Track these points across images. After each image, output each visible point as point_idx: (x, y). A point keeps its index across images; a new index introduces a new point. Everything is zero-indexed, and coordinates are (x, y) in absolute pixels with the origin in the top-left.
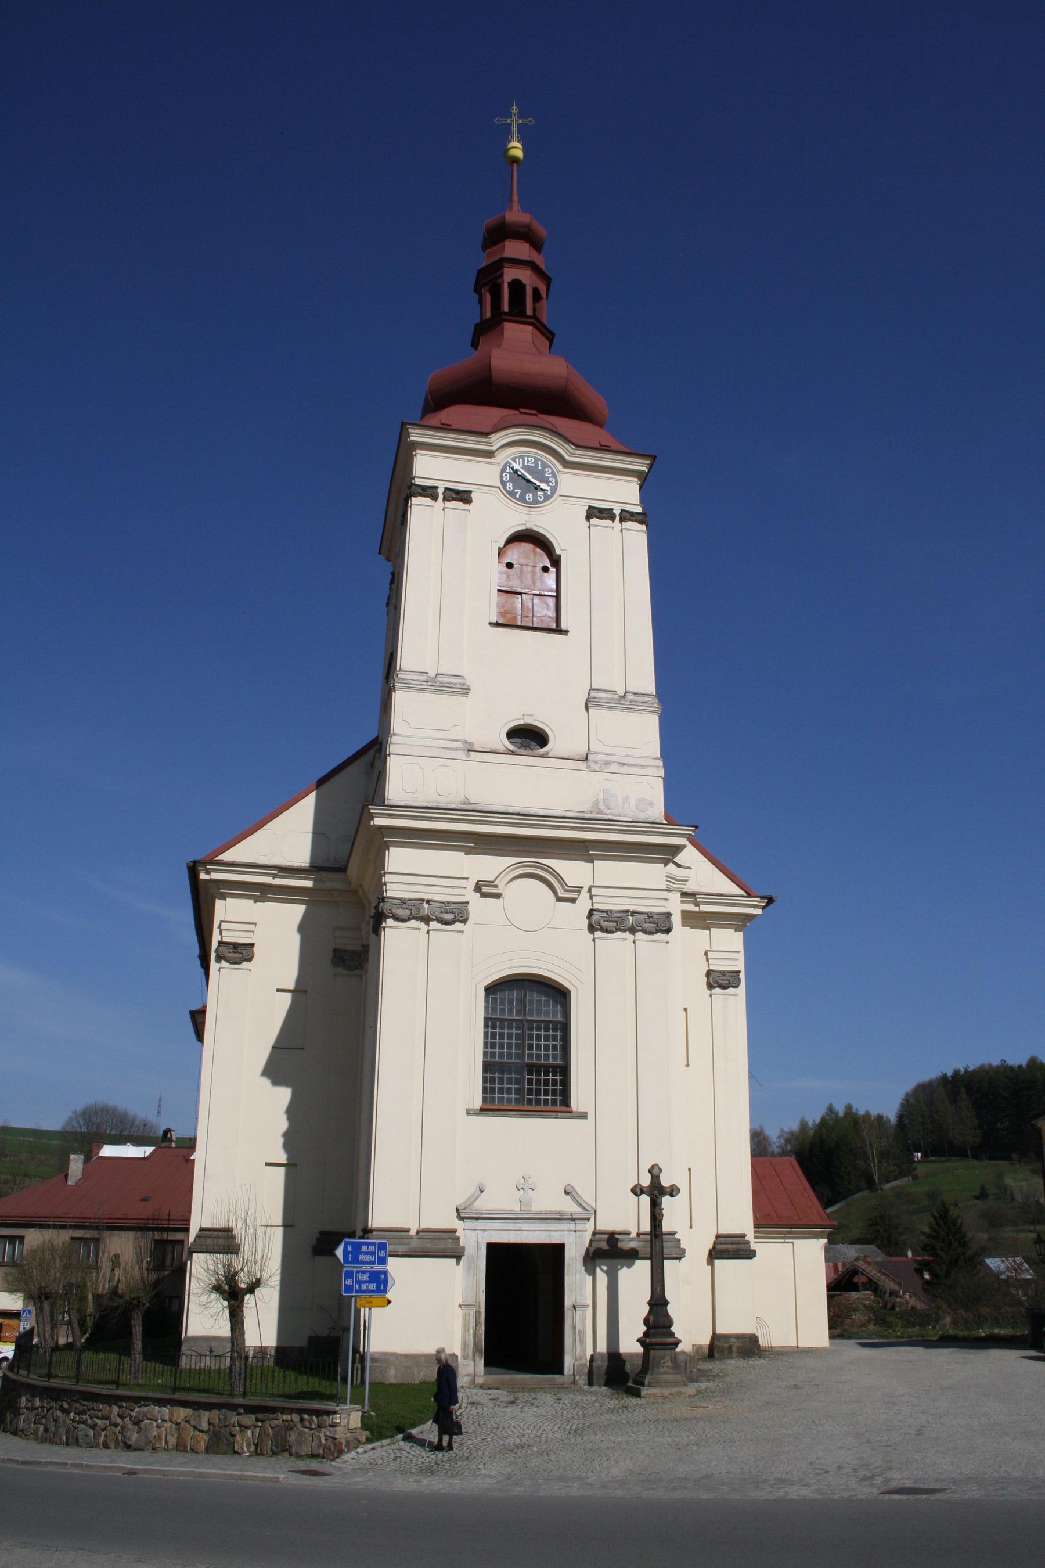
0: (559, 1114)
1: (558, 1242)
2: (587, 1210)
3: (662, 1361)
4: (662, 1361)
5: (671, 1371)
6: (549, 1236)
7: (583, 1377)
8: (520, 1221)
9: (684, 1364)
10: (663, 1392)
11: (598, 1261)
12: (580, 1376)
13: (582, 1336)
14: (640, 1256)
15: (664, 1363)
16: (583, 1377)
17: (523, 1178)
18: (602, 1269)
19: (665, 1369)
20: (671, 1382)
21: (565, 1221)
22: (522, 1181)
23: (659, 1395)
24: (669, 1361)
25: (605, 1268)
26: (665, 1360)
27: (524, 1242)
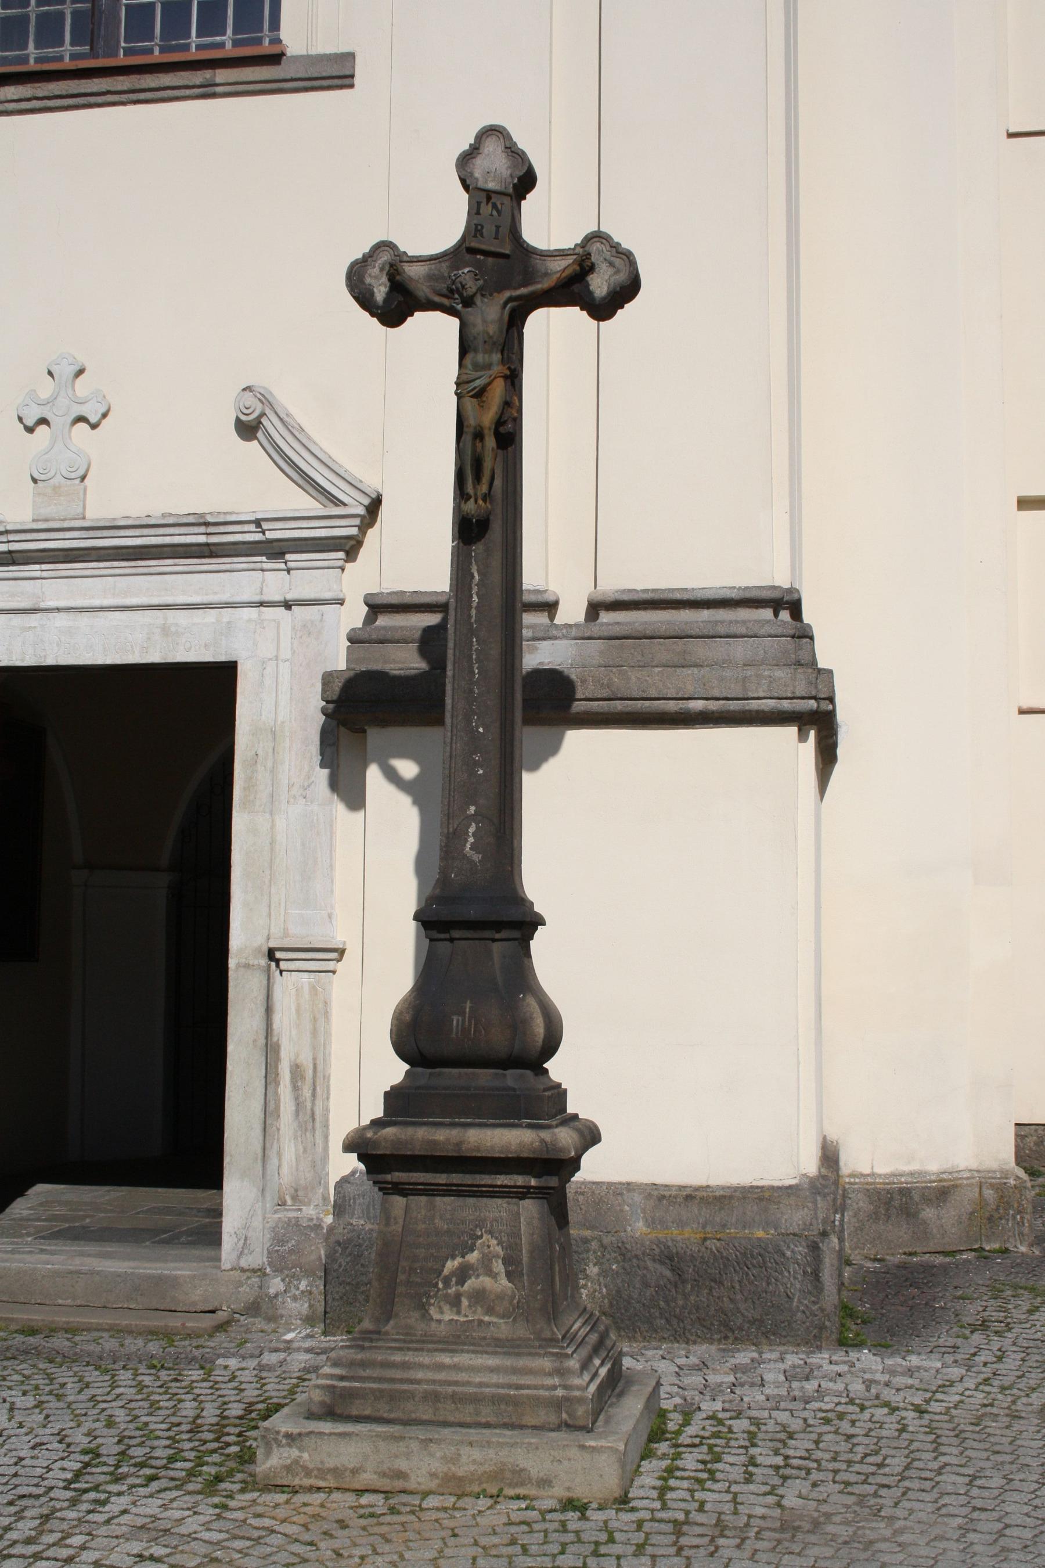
0: (222, 75)
1: (222, 658)
2: (337, 502)
3: (451, 1265)
4: (451, 1265)
5: (502, 1328)
6: (165, 630)
7: (303, 1285)
8: (34, 570)
9: (801, 1249)
10: (402, 1465)
11: (375, 736)
12: (290, 1280)
13: (307, 1093)
14: (578, 707)
15: (463, 1274)
16: (303, 1285)
17: (50, 373)
18: (392, 776)
19: (468, 1314)
20: (476, 1400)
21: (240, 562)
22: (46, 388)
23: (367, 1478)
24: (499, 1267)
25: (408, 769)
26: (473, 1257)
27: (50, 661)
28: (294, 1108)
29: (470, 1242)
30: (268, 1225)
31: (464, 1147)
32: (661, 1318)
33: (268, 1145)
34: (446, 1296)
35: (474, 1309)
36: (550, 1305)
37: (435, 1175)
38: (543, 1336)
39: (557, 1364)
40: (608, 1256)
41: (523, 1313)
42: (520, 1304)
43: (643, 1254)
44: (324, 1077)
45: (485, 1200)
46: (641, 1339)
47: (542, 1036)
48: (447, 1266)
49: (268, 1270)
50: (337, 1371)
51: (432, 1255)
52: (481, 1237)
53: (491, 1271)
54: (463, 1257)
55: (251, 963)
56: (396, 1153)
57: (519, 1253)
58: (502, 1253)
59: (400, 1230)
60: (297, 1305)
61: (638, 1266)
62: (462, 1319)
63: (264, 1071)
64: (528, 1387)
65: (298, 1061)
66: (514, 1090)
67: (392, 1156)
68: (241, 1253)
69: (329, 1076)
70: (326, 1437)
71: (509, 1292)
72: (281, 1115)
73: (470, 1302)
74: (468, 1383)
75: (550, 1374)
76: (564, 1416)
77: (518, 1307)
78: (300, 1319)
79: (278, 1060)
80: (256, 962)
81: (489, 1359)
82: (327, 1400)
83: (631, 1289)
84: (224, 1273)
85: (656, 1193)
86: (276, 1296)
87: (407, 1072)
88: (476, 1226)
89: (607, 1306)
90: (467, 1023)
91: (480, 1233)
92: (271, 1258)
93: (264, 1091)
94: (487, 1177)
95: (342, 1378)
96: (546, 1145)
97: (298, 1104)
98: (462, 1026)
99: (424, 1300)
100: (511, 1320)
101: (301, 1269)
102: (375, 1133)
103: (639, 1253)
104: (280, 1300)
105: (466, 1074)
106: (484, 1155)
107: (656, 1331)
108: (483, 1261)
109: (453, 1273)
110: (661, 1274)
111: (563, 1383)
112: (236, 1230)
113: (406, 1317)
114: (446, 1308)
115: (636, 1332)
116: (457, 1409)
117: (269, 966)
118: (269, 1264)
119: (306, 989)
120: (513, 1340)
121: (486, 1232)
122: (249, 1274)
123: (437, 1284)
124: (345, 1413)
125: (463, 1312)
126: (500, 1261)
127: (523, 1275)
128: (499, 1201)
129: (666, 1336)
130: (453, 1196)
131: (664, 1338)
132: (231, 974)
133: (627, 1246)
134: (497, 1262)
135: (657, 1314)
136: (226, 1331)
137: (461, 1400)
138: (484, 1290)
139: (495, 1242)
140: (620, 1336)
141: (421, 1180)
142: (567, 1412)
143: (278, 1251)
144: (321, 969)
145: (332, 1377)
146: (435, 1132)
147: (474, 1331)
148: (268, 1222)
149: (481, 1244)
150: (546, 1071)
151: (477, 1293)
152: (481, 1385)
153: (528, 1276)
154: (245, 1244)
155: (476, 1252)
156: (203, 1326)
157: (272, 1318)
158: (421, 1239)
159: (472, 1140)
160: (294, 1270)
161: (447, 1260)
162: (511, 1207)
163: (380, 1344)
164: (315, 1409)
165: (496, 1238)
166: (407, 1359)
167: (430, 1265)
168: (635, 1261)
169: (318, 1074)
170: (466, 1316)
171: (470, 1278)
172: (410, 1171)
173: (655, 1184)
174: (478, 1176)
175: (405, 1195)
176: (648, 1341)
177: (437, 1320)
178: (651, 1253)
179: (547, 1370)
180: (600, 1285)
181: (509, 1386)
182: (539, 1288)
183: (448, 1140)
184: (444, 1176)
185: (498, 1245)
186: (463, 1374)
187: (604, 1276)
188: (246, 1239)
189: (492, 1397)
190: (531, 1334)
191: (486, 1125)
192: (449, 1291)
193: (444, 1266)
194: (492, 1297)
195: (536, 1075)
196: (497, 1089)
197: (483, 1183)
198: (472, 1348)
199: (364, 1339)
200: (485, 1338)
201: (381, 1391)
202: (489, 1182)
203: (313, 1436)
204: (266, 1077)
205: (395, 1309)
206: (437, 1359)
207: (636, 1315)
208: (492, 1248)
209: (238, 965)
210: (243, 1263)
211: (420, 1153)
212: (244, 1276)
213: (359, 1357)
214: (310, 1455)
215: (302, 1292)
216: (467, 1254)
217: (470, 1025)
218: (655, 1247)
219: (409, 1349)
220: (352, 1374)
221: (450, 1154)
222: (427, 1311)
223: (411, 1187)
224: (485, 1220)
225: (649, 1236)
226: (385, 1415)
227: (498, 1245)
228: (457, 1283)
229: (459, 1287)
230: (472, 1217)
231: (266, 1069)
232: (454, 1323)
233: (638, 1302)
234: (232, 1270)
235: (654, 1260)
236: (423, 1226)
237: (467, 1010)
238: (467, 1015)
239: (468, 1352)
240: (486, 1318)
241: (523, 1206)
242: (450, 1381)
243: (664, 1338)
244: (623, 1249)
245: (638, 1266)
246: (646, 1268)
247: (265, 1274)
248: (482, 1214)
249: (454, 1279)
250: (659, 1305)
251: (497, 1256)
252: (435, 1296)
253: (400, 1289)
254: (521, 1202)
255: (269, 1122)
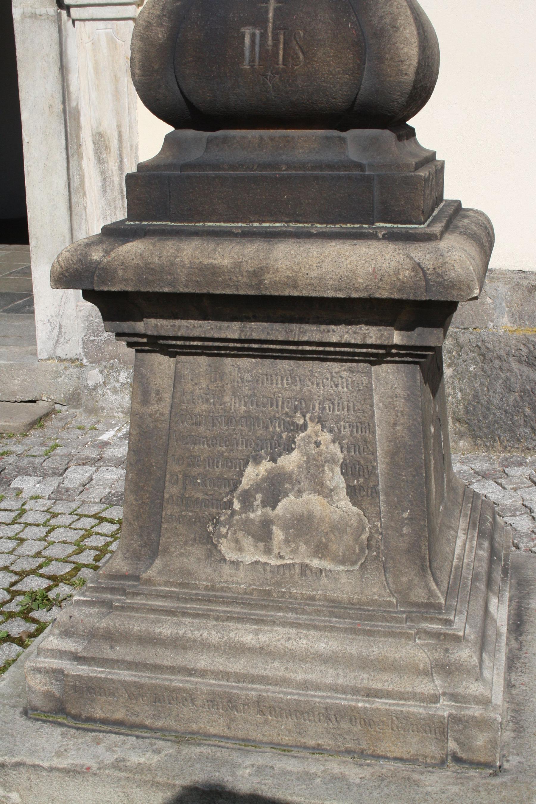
28: (100, 184)
29: (284, 435)
30: (81, 314)
31: (267, 279)
32: (525, 427)
33: (75, 226)
34: (247, 522)
35: (293, 545)
36: (424, 545)
37: (218, 324)
38: (413, 599)
39: (438, 655)
40: (464, 357)
41: (377, 557)
42: (373, 543)
43: (508, 354)
44: (131, 146)
45: (309, 365)
46: (500, 449)
47: (414, 62)
48: (246, 474)
49: (85, 361)
50: (69, 645)
51: (222, 454)
52: (304, 427)
53: (322, 484)
54: (274, 460)
55: (38, 12)
56: (143, 290)
57: (371, 457)
58: (340, 456)
59: (167, 411)
60: (118, 398)
61: (501, 368)
62: (274, 562)
63: (64, 142)
64: (388, 695)
65: (101, 130)
66: (360, 166)
67: (138, 294)
68: (57, 342)
69: (137, 145)
70: (44, 773)
71: (354, 522)
72: (87, 193)
73: (287, 534)
74: (284, 682)
75: (427, 673)
76: (452, 745)
77: (369, 547)
78: (122, 412)
79: (79, 128)
80: (43, 11)
81: (319, 640)
82: (56, 690)
83: (491, 393)
84: (41, 362)
85: (525, 283)
86: (95, 388)
87: (168, 138)
88: (296, 409)
89: (462, 412)
90: (270, 42)
91: (301, 422)
92: (87, 348)
93: (66, 165)
94: (313, 328)
95: (77, 658)
96: (425, 274)
97: (105, 179)
98: (262, 45)
99: (211, 528)
100: (357, 567)
101: (119, 360)
102: (107, 253)
103: (502, 353)
104: (100, 392)
105: (272, 139)
106: (305, 293)
107: (519, 440)
108: (308, 468)
109: (257, 487)
110: (528, 377)
111: (449, 691)
112: (49, 318)
113: (181, 555)
114: (247, 542)
115: (495, 441)
116: (266, 722)
117: (59, 15)
118: (85, 355)
119: (103, 41)
120: (360, 603)
121: (311, 419)
122: (66, 364)
123: (230, 504)
124: (84, 715)
125: (276, 551)
126: (338, 469)
127: (377, 493)
128: (335, 367)
129: (530, 446)
130: (254, 357)
131: (529, 449)
132: (17, 27)
133: (489, 346)
134: (332, 470)
135: (521, 422)
136: (42, 427)
137: (272, 709)
138: (310, 516)
139: (326, 437)
140: (476, 445)
141: (196, 333)
142: (456, 740)
143: (93, 341)
144: (118, 16)
145: (62, 654)
146: (215, 250)
147: (295, 584)
148: (80, 311)
149: (303, 439)
150: (411, 132)
151: (298, 520)
152: (305, 685)
153: (387, 495)
154: (60, 332)
155: (295, 453)
156: (15, 425)
157: (91, 411)
158: (202, 429)
159: (282, 265)
160: (112, 361)
161: (246, 464)
162: (356, 377)
163: (139, 600)
164: (38, 702)
165: (331, 431)
166: (181, 632)
167: (217, 471)
168: (497, 362)
169: (124, 144)
170: (282, 557)
171: (286, 495)
172: (175, 317)
173: (523, 272)
174: (295, 327)
175: (173, 355)
176: (509, 451)
177: (233, 562)
178: (517, 354)
179: (421, 666)
180: (454, 389)
181: (355, 691)
182: (405, 515)
183: (238, 265)
184: (236, 326)
185: (334, 441)
186: (277, 664)
187: (460, 379)
188: (60, 327)
189: (326, 709)
190: (392, 593)
191: (307, 235)
192: (252, 515)
193: (241, 474)
194: (324, 527)
195: (400, 138)
196: (330, 166)
197: (305, 338)
198: (291, 616)
199: (113, 590)
200: (312, 598)
201: (139, 686)
202: (317, 338)
203: (23, 770)
204: (67, 148)
205: (162, 540)
206: (232, 635)
207: (496, 422)
208: (322, 447)
209: (24, 16)
210: (60, 352)
211: (186, 290)
212: (62, 366)
213: (103, 624)
214: (21, 796)
215: (123, 384)
216: (280, 455)
217: (276, 45)
218: (522, 347)
219: (185, 614)
220: (91, 655)
221: (241, 292)
222: (215, 546)
223: (179, 343)
224: (311, 399)
225: (516, 334)
226: (148, 722)
227: (334, 441)
228: (264, 504)
229: (269, 509)
230: (287, 394)
231: (66, 139)
232: (259, 567)
233: (500, 409)
234: (49, 359)
235: (520, 362)
236: (205, 407)
237: (271, 15)
238: (270, 25)
239: (284, 624)
240: (315, 563)
241: (378, 375)
242: (253, 676)
243: (529, 449)
244: (483, 348)
245: (501, 368)
246: (511, 371)
247: (82, 366)
248: (305, 389)
249: (259, 497)
250: (523, 412)
251: (333, 461)
252: (229, 522)
253: (169, 510)
254: (373, 368)
255: (74, 200)
